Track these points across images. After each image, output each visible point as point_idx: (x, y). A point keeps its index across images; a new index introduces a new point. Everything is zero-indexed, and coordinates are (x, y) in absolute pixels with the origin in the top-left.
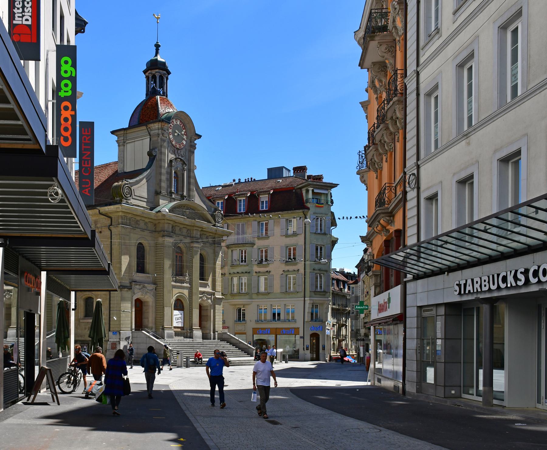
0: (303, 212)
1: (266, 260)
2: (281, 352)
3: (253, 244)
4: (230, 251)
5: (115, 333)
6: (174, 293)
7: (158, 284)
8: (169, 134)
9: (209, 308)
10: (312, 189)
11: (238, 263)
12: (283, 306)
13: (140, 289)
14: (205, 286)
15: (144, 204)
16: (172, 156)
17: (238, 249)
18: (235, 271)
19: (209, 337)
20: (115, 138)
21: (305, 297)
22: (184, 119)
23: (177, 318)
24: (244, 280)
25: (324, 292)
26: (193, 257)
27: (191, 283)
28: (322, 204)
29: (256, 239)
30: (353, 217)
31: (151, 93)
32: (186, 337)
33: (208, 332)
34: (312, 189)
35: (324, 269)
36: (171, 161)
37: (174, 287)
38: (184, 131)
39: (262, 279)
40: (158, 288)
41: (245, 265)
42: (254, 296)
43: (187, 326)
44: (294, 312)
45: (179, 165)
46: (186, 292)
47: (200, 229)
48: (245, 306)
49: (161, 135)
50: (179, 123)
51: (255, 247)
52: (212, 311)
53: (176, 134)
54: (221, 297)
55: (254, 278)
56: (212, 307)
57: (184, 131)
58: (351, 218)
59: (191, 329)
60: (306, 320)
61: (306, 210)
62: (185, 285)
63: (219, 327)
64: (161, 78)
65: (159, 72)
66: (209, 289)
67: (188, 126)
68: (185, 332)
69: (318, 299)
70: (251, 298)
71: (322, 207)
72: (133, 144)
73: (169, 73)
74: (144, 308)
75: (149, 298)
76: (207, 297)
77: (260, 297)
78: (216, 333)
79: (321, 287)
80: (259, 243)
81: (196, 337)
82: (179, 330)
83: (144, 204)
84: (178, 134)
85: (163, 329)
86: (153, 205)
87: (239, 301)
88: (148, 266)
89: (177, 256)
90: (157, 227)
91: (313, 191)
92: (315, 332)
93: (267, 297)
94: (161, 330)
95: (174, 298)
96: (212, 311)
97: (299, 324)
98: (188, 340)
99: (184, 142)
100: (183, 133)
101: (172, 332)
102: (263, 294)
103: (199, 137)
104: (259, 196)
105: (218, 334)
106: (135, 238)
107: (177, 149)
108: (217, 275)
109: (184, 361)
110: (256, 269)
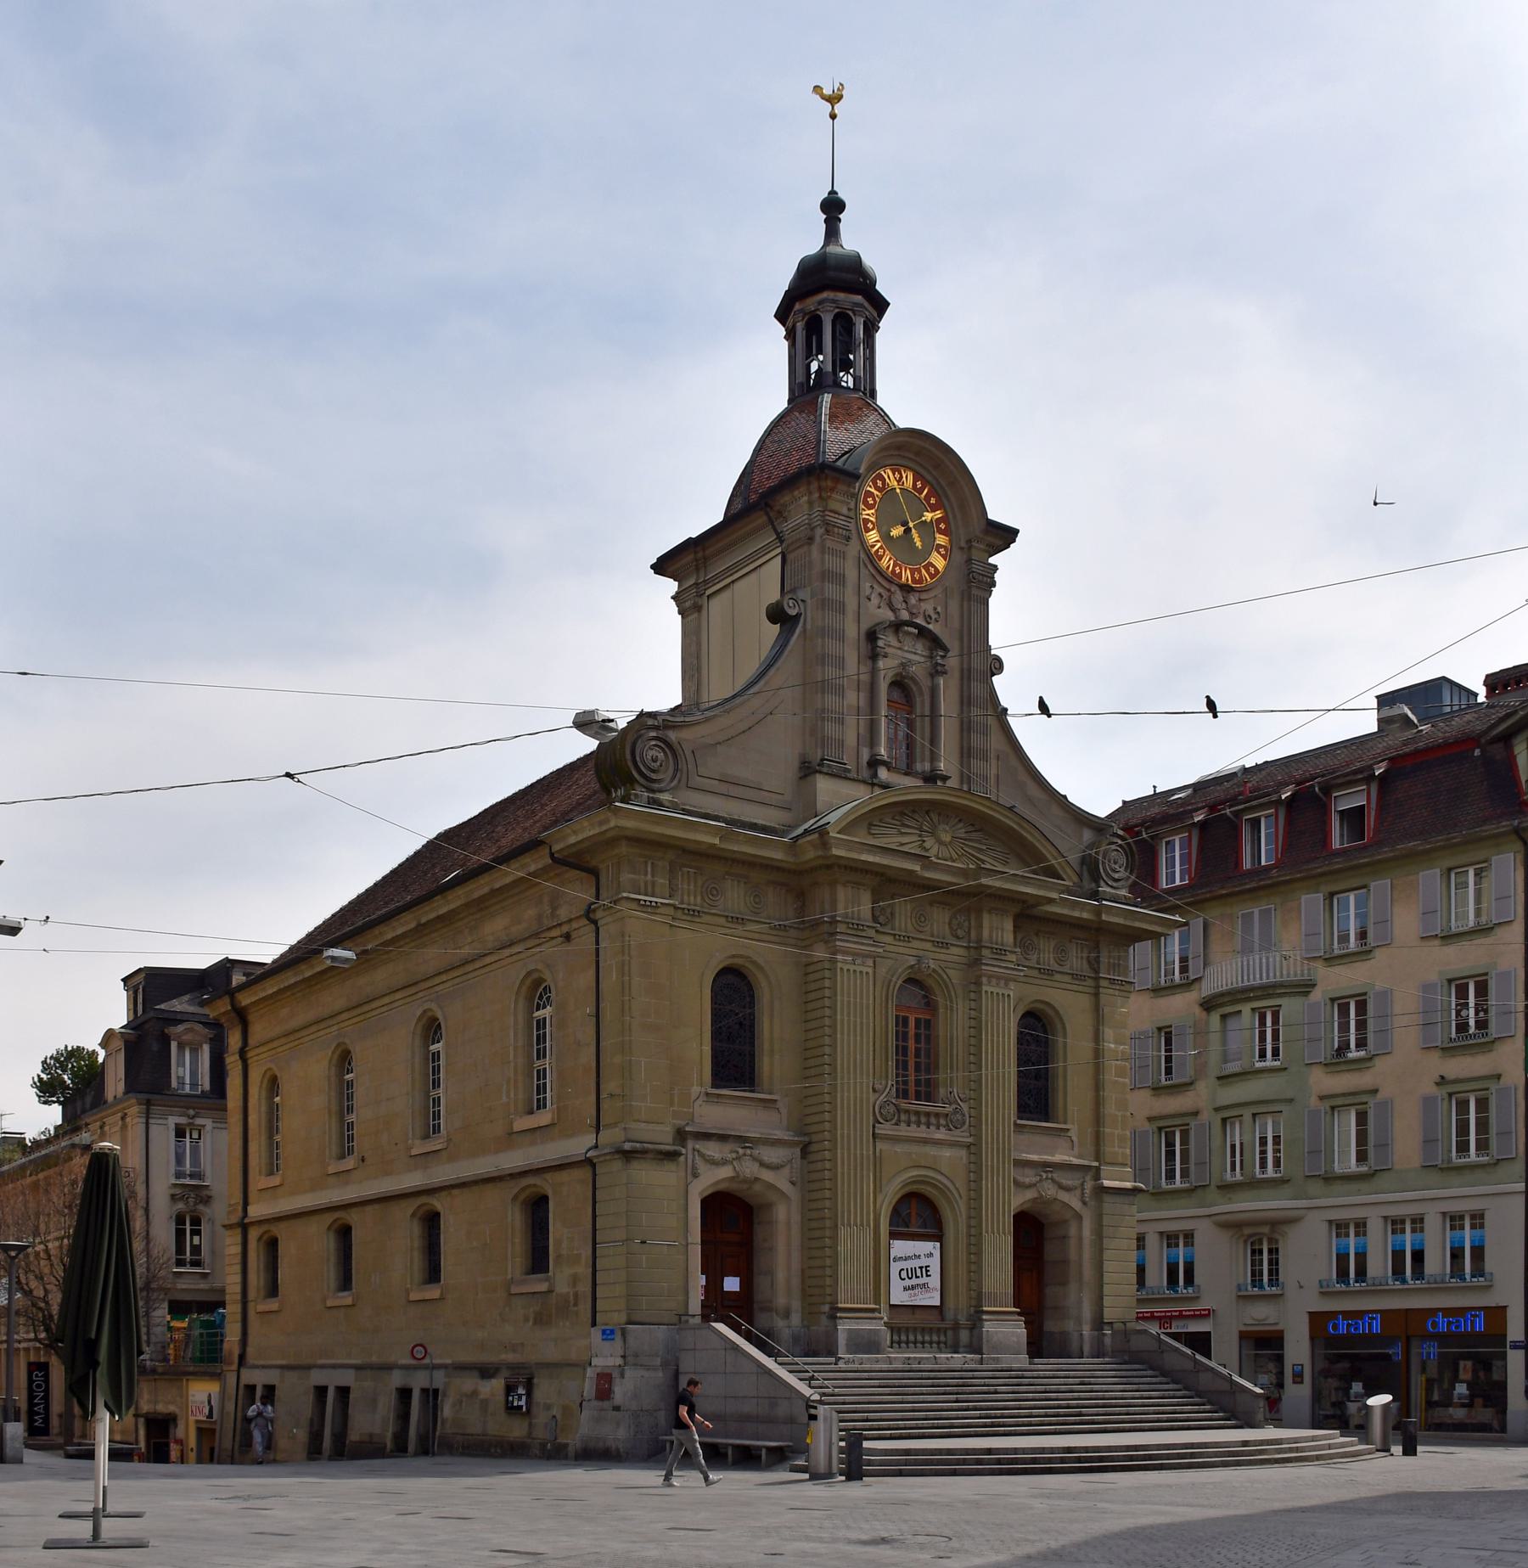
2: (1386, 1407)
3: (1304, 988)
5: (608, 1334)
19: (1075, 1346)
20: (671, 586)
22: (935, 465)
23: (915, 1271)
31: (803, 392)
44: (1364, 1254)
64: (843, 322)
65: (834, 301)
72: (726, 595)
73: (881, 305)
75: (773, 1175)
81: (997, 1349)
85: (833, 1317)
88: (766, 1060)
89: (902, 1022)
94: (824, 1320)
101: (879, 1326)
103: (1005, 536)
107: (906, 589)
109: (841, 1450)
110: (1324, 1082)
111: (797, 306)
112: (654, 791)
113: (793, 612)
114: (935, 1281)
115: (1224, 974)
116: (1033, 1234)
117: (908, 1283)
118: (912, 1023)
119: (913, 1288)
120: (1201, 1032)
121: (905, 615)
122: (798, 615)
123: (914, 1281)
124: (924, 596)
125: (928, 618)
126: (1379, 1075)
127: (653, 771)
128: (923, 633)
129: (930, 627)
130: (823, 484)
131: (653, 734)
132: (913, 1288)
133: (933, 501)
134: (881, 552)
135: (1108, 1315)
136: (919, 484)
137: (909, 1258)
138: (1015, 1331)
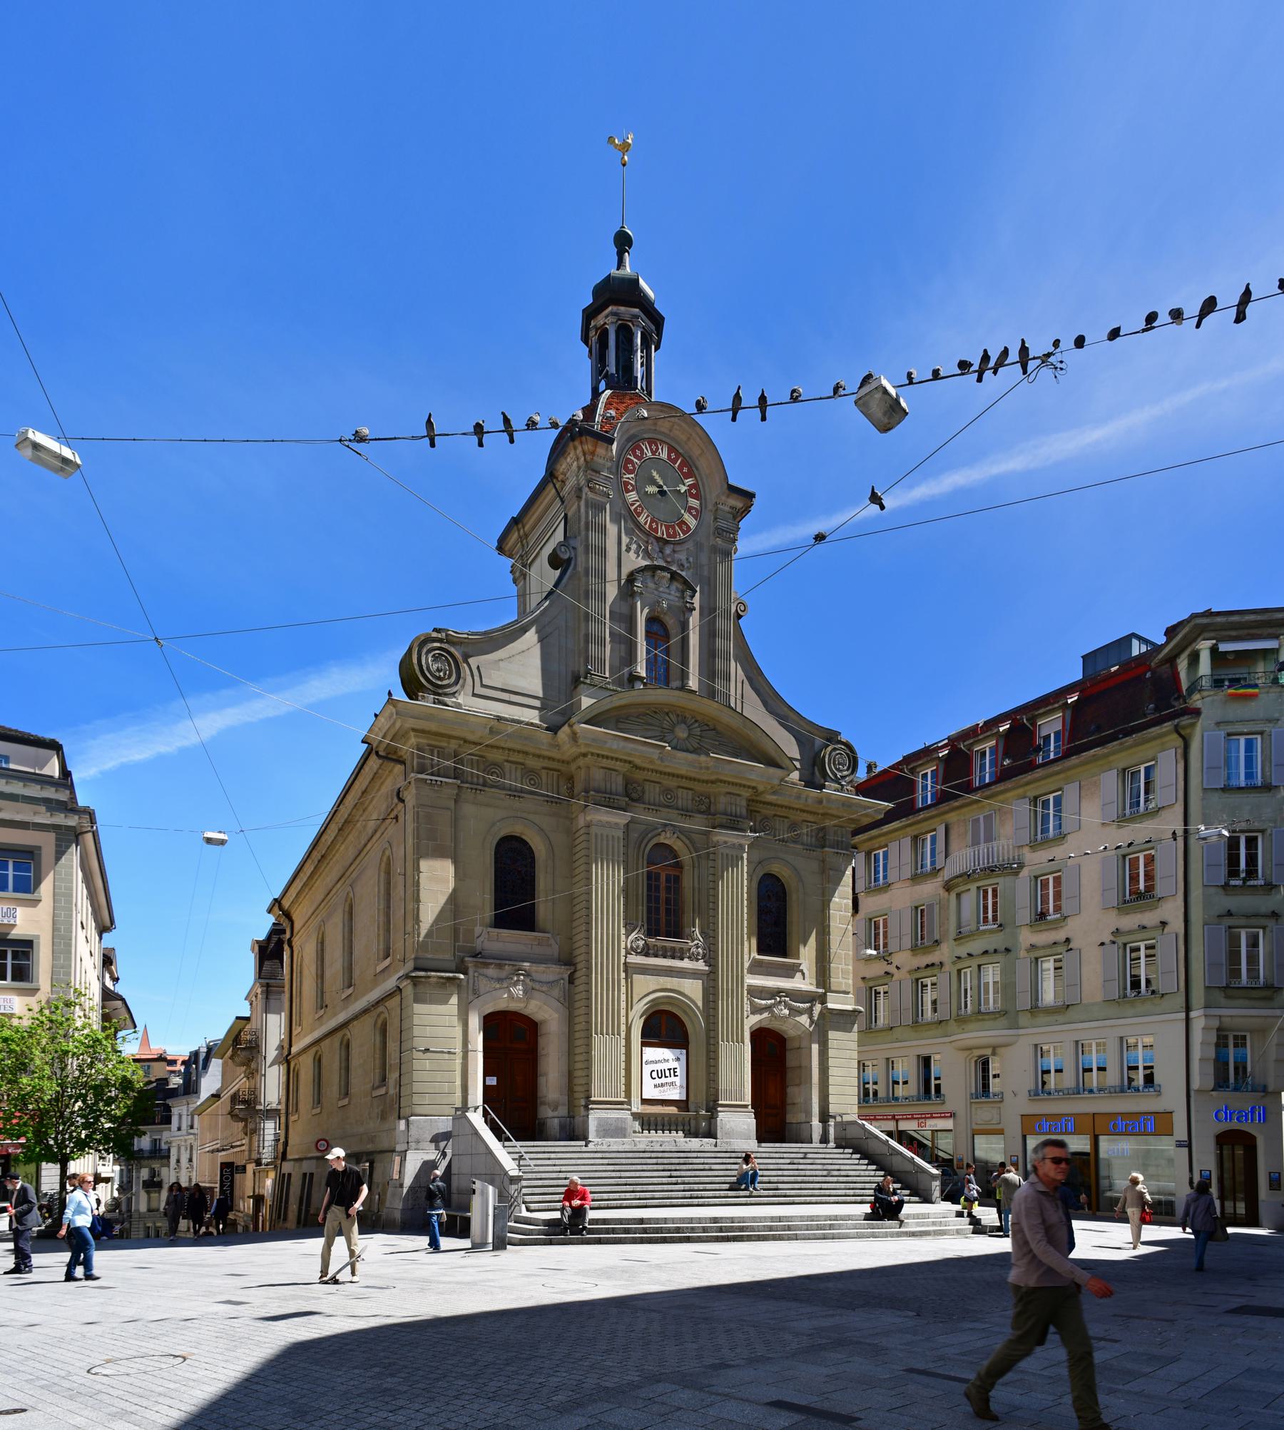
0: (1177, 730)
1: (1058, 909)
4: (953, 895)
6: (639, 990)
7: (572, 964)
8: (625, 487)
9: (804, 1044)
10: (1209, 643)
11: (973, 927)
12: (1113, 1047)
13: (499, 980)
14: (790, 972)
15: (532, 716)
16: (635, 561)
17: (973, 887)
18: (962, 951)
21: (1188, 1009)
23: (661, 1073)
24: (991, 974)
25: (1269, 987)
26: (716, 878)
27: (711, 957)
28: (1256, 686)
29: (1026, 850)
30: (1096, 335)
32: (690, 1133)
33: (802, 1117)
34: (1209, 643)
35: (1263, 910)
36: (631, 578)
37: (644, 970)
38: (689, 481)
39: (1049, 965)
40: (578, 974)
41: (991, 931)
42: (1024, 1019)
43: (699, 1097)
45: (669, 597)
46: (693, 989)
47: (746, 794)
48: (999, 1050)
49: (586, 490)
50: (664, 456)
51: (1025, 873)
52: (815, 1047)
53: (652, 489)
54: (850, 1008)
55: (1023, 968)
56: (815, 1037)
57: (689, 481)
58: (1080, 342)
59: (713, 1108)
60: (1195, 1084)
61: (1185, 721)
62: (686, 964)
63: (845, 1102)
66: (804, 983)
67: (703, 464)
68: (695, 1115)
69: (1238, 1014)
70: (1016, 1026)
71: (1254, 696)
73: (657, 320)
74: (542, 1041)
75: (545, 1011)
76: (791, 1009)
77: (1042, 1019)
78: (832, 1123)
79: (1253, 973)
80: (1036, 860)
81: (729, 1134)
82: (673, 1110)
83: (532, 716)
84: (662, 493)
85: (587, 1108)
86: (557, 710)
87: (979, 1035)
90: (565, 786)
91: (1214, 650)
92: (1234, 1125)
93: (1060, 1018)
95: (640, 1007)
96: (815, 1047)
97: (1171, 1097)
98: (695, 1143)
99: (692, 522)
100: (683, 489)
101: (626, 1115)
102: (1050, 1011)
104: (1034, 724)
105: (836, 1124)
106: (486, 820)
107: (658, 539)
108: (835, 938)
110: (1027, 937)
111: (593, 324)
112: (439, 695)
113: (566, 557)
114: (679, 1080)
115: (962, 858)
116: (772, 1054)
117: (658, 1081)
118: (663, 878)
119: (662, 1085)
120: (943, 906)
121: (661, 563)
122: (569, 560)
123: (664, 1080)
124: (678, 548)
125: (681, 566)
126: (1073, 928)
127: (439, 678)
128: (674, 576)
129: (683, 574)
130: (586, 447)
131: (437, 645)
132: (662, 1085)
133: (685, 470)
134: (639, 510)
135: (833, 1109)
136: (673, 456)
137: (660, 1061)
138: (747, 1122)
